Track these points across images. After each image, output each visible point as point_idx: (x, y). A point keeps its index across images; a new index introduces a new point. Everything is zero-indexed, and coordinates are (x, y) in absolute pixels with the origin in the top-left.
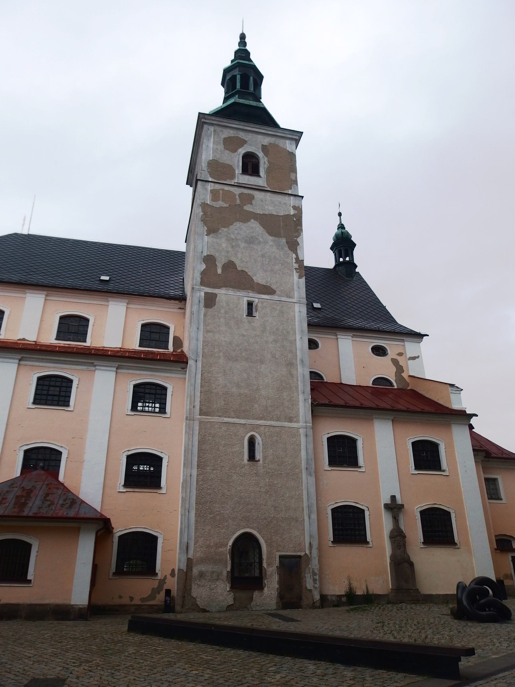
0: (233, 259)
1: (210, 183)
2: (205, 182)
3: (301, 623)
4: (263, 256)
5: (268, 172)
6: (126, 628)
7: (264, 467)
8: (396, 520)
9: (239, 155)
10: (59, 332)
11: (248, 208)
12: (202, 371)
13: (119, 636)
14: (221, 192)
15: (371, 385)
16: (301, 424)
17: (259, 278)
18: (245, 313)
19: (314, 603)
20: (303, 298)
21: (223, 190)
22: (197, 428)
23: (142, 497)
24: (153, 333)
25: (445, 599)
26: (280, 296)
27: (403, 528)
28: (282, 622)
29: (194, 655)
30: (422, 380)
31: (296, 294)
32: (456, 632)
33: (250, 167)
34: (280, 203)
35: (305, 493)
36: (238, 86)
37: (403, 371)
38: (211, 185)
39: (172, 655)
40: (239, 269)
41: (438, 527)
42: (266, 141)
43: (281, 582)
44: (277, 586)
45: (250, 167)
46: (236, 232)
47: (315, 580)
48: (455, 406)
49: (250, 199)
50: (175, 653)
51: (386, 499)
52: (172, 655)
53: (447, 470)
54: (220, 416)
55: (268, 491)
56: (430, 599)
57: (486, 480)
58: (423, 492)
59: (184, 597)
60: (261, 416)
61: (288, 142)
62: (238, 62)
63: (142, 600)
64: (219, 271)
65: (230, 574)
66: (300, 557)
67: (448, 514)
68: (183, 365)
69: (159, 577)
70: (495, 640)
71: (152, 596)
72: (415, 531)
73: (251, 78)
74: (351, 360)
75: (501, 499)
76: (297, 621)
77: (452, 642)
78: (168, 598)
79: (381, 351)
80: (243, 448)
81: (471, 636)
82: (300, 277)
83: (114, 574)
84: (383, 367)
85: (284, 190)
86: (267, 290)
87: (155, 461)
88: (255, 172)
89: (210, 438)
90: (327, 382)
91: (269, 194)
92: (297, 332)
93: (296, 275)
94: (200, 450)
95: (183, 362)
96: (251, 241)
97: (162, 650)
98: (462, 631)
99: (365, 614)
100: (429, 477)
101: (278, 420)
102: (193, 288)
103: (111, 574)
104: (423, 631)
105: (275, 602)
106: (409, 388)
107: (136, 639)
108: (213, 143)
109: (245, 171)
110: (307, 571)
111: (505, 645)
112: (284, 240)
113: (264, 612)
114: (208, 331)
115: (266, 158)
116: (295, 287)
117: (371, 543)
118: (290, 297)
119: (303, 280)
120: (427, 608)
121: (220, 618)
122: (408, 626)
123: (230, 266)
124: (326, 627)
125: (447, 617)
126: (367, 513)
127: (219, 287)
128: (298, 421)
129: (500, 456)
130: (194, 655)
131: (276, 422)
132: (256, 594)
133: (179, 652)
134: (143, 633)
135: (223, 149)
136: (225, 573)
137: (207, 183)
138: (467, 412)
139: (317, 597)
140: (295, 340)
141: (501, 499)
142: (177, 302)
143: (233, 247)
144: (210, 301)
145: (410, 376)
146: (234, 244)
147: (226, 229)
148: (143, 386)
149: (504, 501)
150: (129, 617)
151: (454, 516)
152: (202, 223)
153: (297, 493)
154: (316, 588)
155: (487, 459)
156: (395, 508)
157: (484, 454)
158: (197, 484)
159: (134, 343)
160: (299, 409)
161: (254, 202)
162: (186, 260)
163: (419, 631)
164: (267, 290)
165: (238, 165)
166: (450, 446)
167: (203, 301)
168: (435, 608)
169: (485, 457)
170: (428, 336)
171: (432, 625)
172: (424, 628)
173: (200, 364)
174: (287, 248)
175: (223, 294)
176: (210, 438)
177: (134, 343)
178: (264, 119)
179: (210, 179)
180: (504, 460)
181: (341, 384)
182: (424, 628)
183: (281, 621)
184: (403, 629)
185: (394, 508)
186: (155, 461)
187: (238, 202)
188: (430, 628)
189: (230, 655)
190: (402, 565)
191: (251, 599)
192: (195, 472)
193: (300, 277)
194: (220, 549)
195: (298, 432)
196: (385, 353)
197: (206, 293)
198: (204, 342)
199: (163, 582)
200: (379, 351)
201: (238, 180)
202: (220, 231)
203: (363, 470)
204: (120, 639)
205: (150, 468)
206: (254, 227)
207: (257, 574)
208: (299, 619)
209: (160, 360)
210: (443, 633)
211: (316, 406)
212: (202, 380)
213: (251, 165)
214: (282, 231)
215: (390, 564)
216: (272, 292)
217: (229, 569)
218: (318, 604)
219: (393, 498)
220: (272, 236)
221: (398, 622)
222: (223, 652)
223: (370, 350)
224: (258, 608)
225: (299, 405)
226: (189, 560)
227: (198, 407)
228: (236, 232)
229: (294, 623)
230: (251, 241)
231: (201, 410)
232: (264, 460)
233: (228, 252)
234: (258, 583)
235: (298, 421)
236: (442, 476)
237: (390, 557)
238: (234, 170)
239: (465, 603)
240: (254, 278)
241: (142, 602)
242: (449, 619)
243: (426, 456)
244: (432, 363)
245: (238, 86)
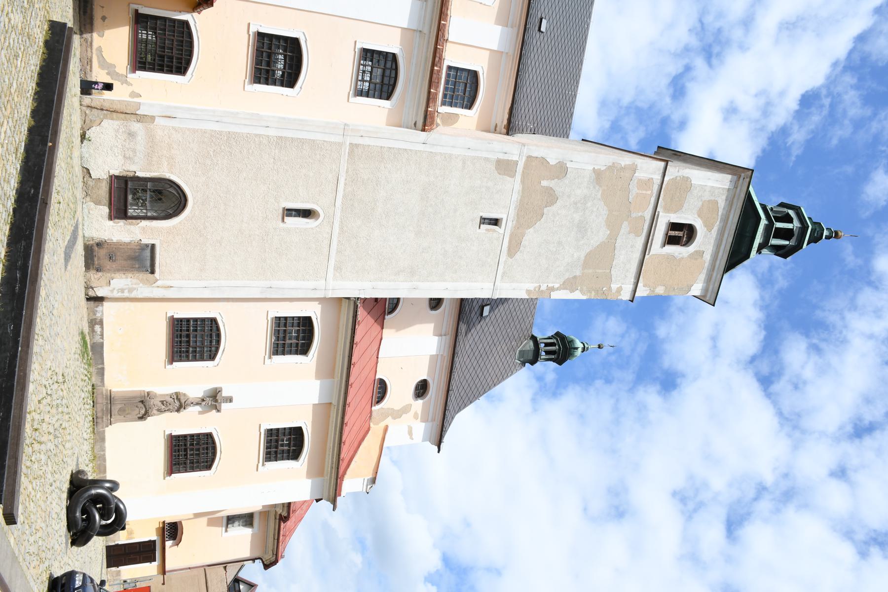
0: (559, 203)
3: (63, 270)
4: (560, 243)
5: (671, 258)
6: (57, 18)
7: (275, 229)
11: (625, 227)
12: (411, 150)
13: (41, 5)
17: (531, 237)
18: (486, 215)
19: (92, 288)
22: (333, 139)
23: (241, 57)
24: (465, 87)
25: (99, 459)
26: (506, 261)
28: (63, 244)
29: (7, 113)
32: (51, 481)
33: (676, 233)
34: (627, 271)
36: (779, 225)
37: (394, 418)
39: (7, 80)
40: (545, 210)
41: (191, 454)
43: (119, 245)
44: (115, 240)
45: (676, 233)
46: (595, 209)
47: (122, 291)
49: (636, 232)
50: (12, 84)
52: (7, 80)
54: (347, 172)
56: (99, 438)
58: (238, 438)
59: (102, 109)
60: (345, 228)
62: (760, 218)
63: (100, 49)
64: (544, 183)
65: (131, 174)
66: (153, 272)
68: (420, 124)
69: (131, 76)
70: (39, 535)
71: (104, 64)
72: (189, 423)
73: (787, 243)
74: (409, 351)
76: (66, 267)
77: (35, 479)
78: (101, 86)
80: (302, 202)
81: (45, 502)
82: (528, 292)
83: (137, 11)
84: (401, 392)
86: (514, 247)
87: (290, 79)
88: (671, 240)
89: (318, 156)
90: (384, 319)
93: (531, 286)
94: (302, 141)
95: (424, 125)
96: (582, 228)
97: (16, 67)
98: (53, 487)
99: (77, 356)
100: (256, 445)
101: (339, 252)
102: (524, 145)
103: (136, 7)
104: (51, 437)
105: (95, 235)
106: (372, 425)
107: (37, 31)
109: (674, 226)
110: (135, 281)
111: (33, 549)
112: (578, 273)
113: (80, 220)
114: (464, 163)
115: (686, 255)
119: (524, 295)
120: (86, 436)
121: (71, 158)
122: (60, 416)
123: (551, 197)
124: (56, 306)
125: (75, 463)
127: (523, 182)
129: (281, 533)
130: (7, 113)
132: (105, 210)
133: (13, 91)
134: (47, 43)
135: (704, 199)
136: (133, 168)
139: (100, 293)
140: (445, 281)
142: (505, 122)
143: (575, 203)
144: (505, 167)
146: (579, 205)
147: (599, 196)
148: (394, 67)
150: (70, 24)
152: (611, 164)
154: (112, 291)
156: (216, 401)
157: (285, 514)
158: (256, 135)
159: (453, 57)
161: (632, 236)
162: (558, 138)
163: (52, 431)
164: (514, 247)
167: (506, 157)
168: (87, 447)
169: (280, 515)
170: (439, 452)
171: (61, 447)
172: (56, 437)
173: (421, 147)
174: (567, 276)
175: (513, 186)
176: (318, 156)
177: (453, 57)
182: (56, 437)
183: (66, 243)
184: (54, 411)
186: (290, 79)
187: (634, 215)
188: (56, 446)
189: (8, 167)
190: (142, 406)
191: (98, 203)
192: (272, 132)
193: (528, 292)
194: (166, 163)
197: (516, 163)
198: (451, 155)
199: (124, 81)
200: (422, 389)
202: (597, 187)
204: (36, 6)
205: (280, 70)
206: (598, 235)
207: (131, 212)
208: (69, 267)
209: (429, 92)
210: (49, 463)
211: (355, 303)
212: (399, 149)
213: (680, 234)
214: (590, 271)
216: (512, 252)
217: (140, 174)
218: (91, 293)
220: (586, 257)
221: (64, 401)
222: (12, 158)
224: (86, 211)
226: (153, 118)
227: (360, 141)
228: (595, 209)
229: (63, 261)
230: (582, 228)
231: (357, 146)
233: (569, 196)
234: (119, 212)
238: (675, 212)
239: (93, 492)
240: (531, 230)
241: (97, 49)
242: (71, 468)
243: (283, 444)
245: (779, 225)
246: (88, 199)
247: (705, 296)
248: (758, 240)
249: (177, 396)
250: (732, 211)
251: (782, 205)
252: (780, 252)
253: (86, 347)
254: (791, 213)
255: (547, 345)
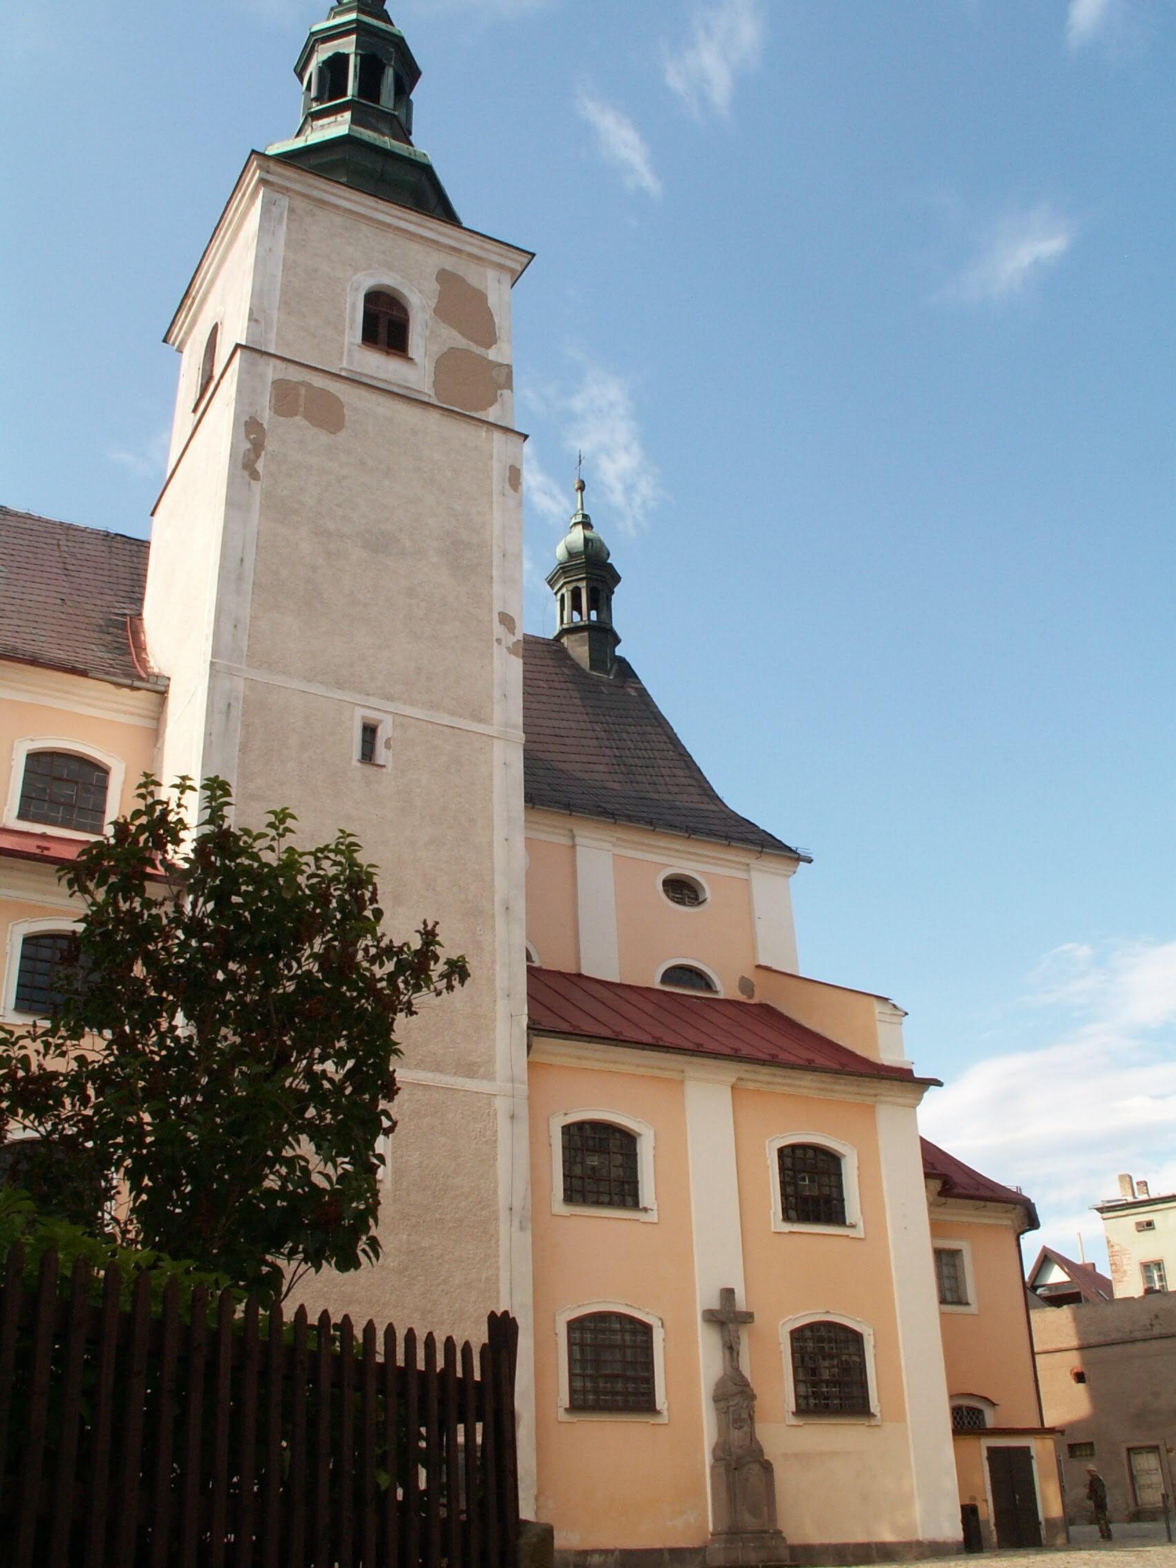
1: (273, 361)
2: (257, 356)
8: (731, 1349)
9: (357, 289)
10: (25, 797)
14: (303, 391)
15: (658, 985)
16: (499, 1085)
20: (515, 727)
21: (308, 385)
27: (747, 1373)
30: (780, 977)
31: (498, 713)
33: (383, 332)
35: (504, 1275)
38: (275, 367)
41: (832, 1373)
42: (436, 261)
45: (383, 332)
48: (887, 1058)
51: (706, 1297)
53: (655, 1207)
55: (406, 1268)
57: (939, 1253)
58: (801, 1280)
61: (491, 274)
67: (856, 1338)
72: (778, 1385)
75: (967, 1304)
79: (686, 892)
85: (476, 410)
91: (434, 416)
92: (497, 822)
101: (438, 1068)
108: (286, 245)
109: (371, 336)
116: (497, 694)
117: (665, 1413)
118: (480, 721)
126: (658, 1336)
128: (489, 1076)
131: (430, 1075)
137: (262, 360)
138: (916, 1075)
140: (491, 844)
141: (967, 1304)
145: (759, 967)
149: (973, 1309)
151: (872, 1343)
153: (484, 1276)
155: (943, 1200)
160: (494, 1040)
165: (353, 320)
166: (869, 1163)
178: (421, 191)
179: (436, 402)
180: (982, 1203)
181: (580, 975)
185: (728, 1319)
190: (744, 1469)
195: (490, 1105)
196: (697, 899)
200: (682, 889)
201: (351, 362)
203: (859, 1233)
213: (385, 324)
215: (713, 1468)
219: (728, 1294)
223: (660, 887)
225: (494, 1030)
232: (395, 1182)
233: (314, 569)
235: (489, 1076)
236: (844, 1240)
237: (714, 1451)
243: (812, 1189)
244: (813, 932)
246: (731, 1326)
247: (512, 271)
248: (388, 142)
249: (721, 1397)
250: (333, 200)
251: (300, 72)
252: (407, 84)
253: (997, 1225)
254: (323, 53)
255: (576, 606)
